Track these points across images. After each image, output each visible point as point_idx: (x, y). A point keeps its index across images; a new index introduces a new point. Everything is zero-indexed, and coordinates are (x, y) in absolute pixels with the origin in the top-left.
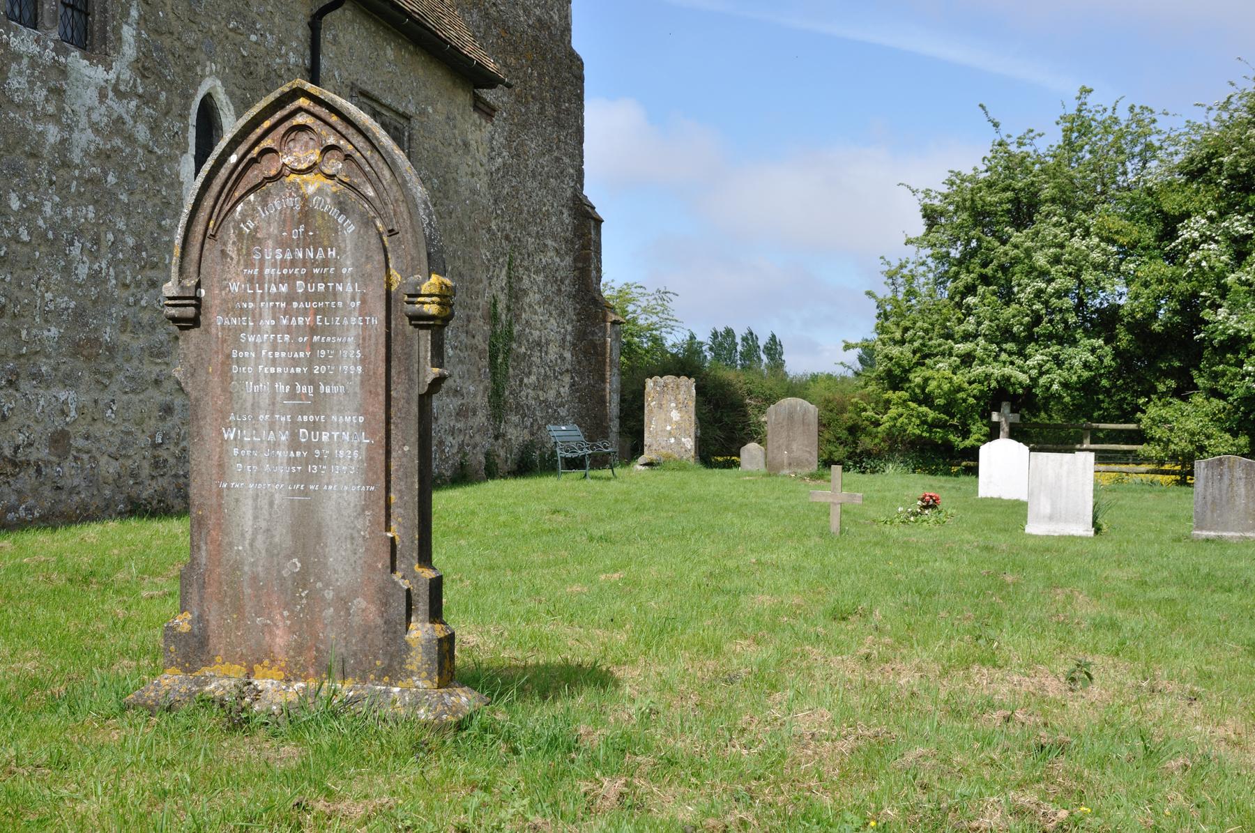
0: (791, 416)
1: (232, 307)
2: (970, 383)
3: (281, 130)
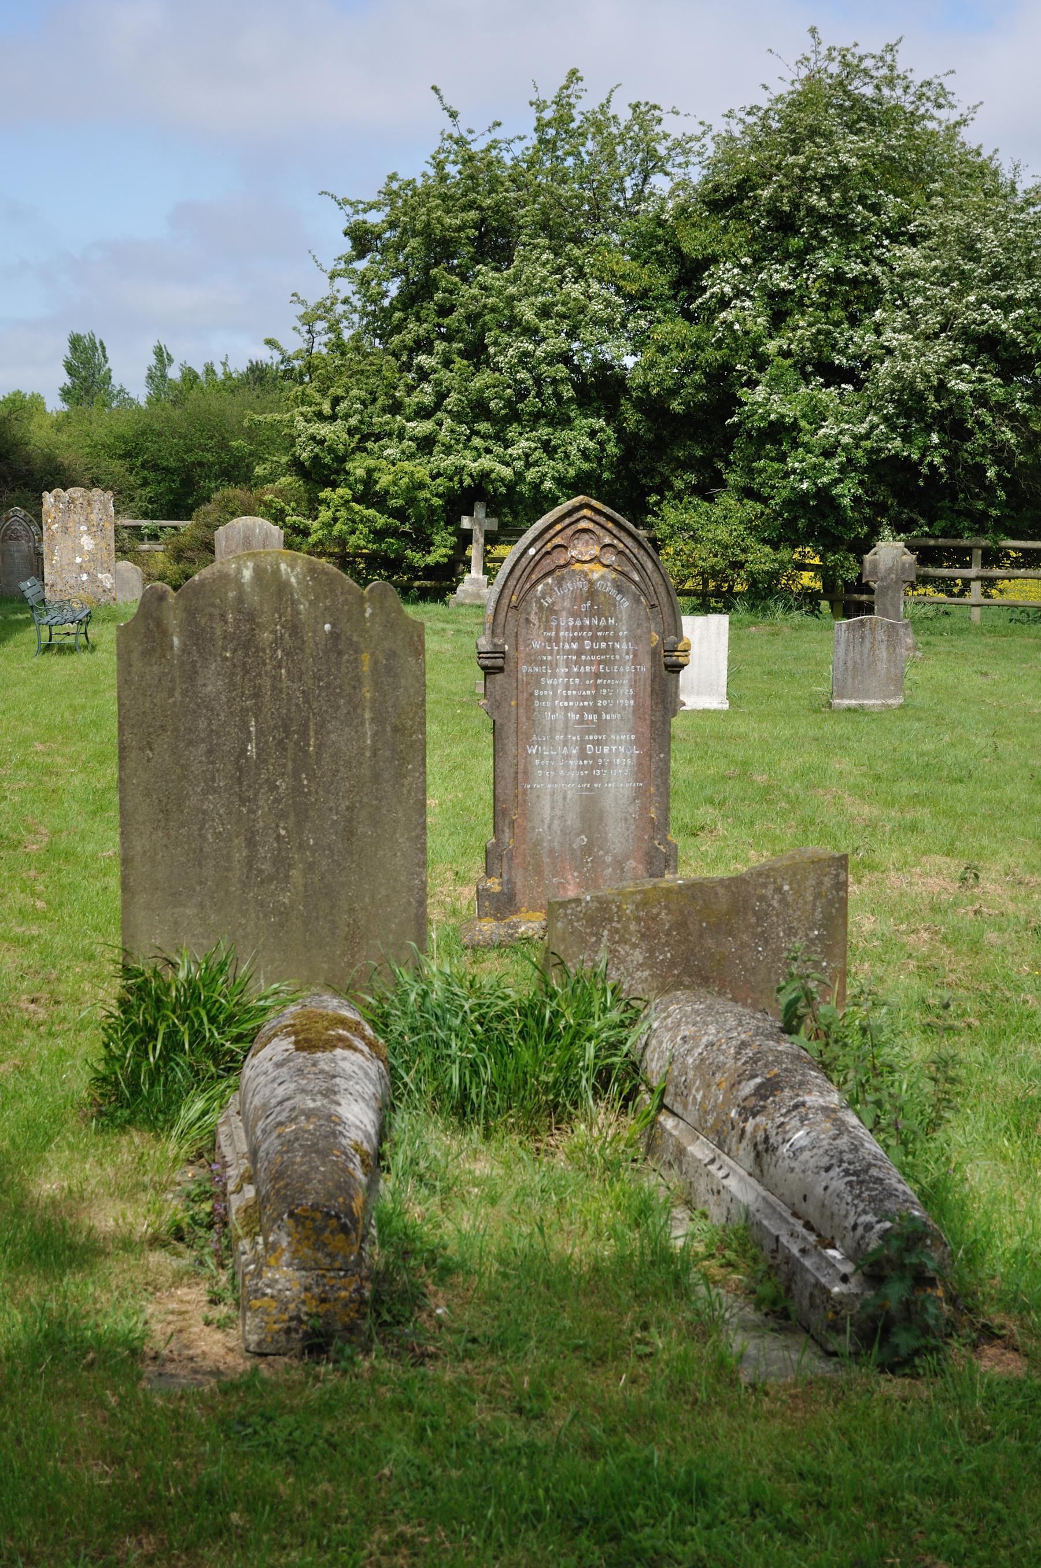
1: (534, 659)
2: (434, 478)
3: (569, 532)
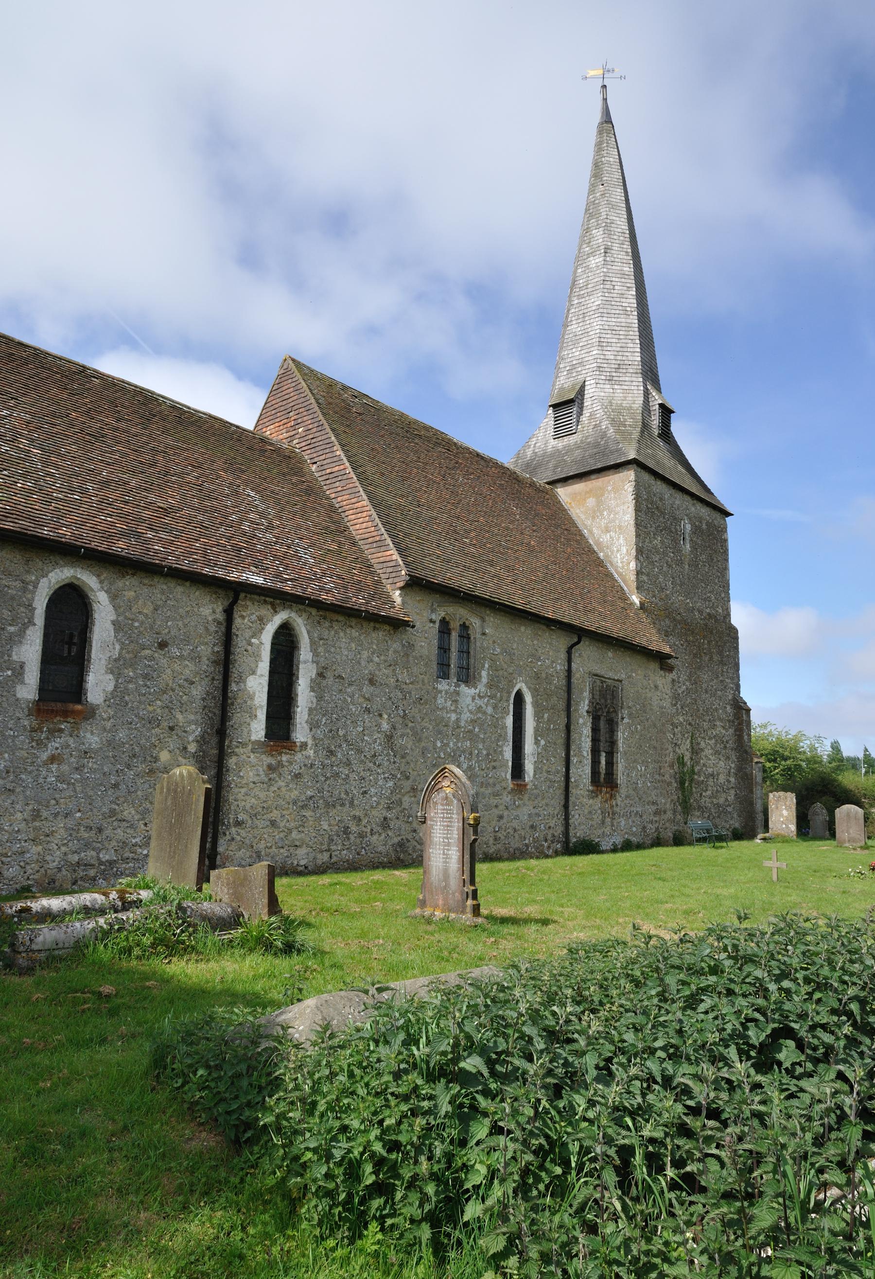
0: (848, 814)
